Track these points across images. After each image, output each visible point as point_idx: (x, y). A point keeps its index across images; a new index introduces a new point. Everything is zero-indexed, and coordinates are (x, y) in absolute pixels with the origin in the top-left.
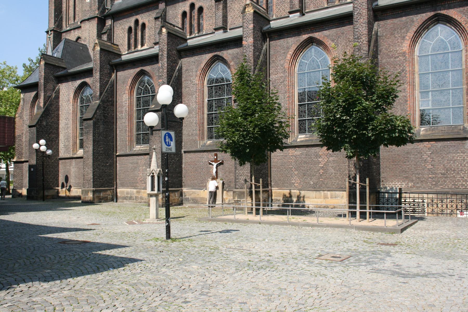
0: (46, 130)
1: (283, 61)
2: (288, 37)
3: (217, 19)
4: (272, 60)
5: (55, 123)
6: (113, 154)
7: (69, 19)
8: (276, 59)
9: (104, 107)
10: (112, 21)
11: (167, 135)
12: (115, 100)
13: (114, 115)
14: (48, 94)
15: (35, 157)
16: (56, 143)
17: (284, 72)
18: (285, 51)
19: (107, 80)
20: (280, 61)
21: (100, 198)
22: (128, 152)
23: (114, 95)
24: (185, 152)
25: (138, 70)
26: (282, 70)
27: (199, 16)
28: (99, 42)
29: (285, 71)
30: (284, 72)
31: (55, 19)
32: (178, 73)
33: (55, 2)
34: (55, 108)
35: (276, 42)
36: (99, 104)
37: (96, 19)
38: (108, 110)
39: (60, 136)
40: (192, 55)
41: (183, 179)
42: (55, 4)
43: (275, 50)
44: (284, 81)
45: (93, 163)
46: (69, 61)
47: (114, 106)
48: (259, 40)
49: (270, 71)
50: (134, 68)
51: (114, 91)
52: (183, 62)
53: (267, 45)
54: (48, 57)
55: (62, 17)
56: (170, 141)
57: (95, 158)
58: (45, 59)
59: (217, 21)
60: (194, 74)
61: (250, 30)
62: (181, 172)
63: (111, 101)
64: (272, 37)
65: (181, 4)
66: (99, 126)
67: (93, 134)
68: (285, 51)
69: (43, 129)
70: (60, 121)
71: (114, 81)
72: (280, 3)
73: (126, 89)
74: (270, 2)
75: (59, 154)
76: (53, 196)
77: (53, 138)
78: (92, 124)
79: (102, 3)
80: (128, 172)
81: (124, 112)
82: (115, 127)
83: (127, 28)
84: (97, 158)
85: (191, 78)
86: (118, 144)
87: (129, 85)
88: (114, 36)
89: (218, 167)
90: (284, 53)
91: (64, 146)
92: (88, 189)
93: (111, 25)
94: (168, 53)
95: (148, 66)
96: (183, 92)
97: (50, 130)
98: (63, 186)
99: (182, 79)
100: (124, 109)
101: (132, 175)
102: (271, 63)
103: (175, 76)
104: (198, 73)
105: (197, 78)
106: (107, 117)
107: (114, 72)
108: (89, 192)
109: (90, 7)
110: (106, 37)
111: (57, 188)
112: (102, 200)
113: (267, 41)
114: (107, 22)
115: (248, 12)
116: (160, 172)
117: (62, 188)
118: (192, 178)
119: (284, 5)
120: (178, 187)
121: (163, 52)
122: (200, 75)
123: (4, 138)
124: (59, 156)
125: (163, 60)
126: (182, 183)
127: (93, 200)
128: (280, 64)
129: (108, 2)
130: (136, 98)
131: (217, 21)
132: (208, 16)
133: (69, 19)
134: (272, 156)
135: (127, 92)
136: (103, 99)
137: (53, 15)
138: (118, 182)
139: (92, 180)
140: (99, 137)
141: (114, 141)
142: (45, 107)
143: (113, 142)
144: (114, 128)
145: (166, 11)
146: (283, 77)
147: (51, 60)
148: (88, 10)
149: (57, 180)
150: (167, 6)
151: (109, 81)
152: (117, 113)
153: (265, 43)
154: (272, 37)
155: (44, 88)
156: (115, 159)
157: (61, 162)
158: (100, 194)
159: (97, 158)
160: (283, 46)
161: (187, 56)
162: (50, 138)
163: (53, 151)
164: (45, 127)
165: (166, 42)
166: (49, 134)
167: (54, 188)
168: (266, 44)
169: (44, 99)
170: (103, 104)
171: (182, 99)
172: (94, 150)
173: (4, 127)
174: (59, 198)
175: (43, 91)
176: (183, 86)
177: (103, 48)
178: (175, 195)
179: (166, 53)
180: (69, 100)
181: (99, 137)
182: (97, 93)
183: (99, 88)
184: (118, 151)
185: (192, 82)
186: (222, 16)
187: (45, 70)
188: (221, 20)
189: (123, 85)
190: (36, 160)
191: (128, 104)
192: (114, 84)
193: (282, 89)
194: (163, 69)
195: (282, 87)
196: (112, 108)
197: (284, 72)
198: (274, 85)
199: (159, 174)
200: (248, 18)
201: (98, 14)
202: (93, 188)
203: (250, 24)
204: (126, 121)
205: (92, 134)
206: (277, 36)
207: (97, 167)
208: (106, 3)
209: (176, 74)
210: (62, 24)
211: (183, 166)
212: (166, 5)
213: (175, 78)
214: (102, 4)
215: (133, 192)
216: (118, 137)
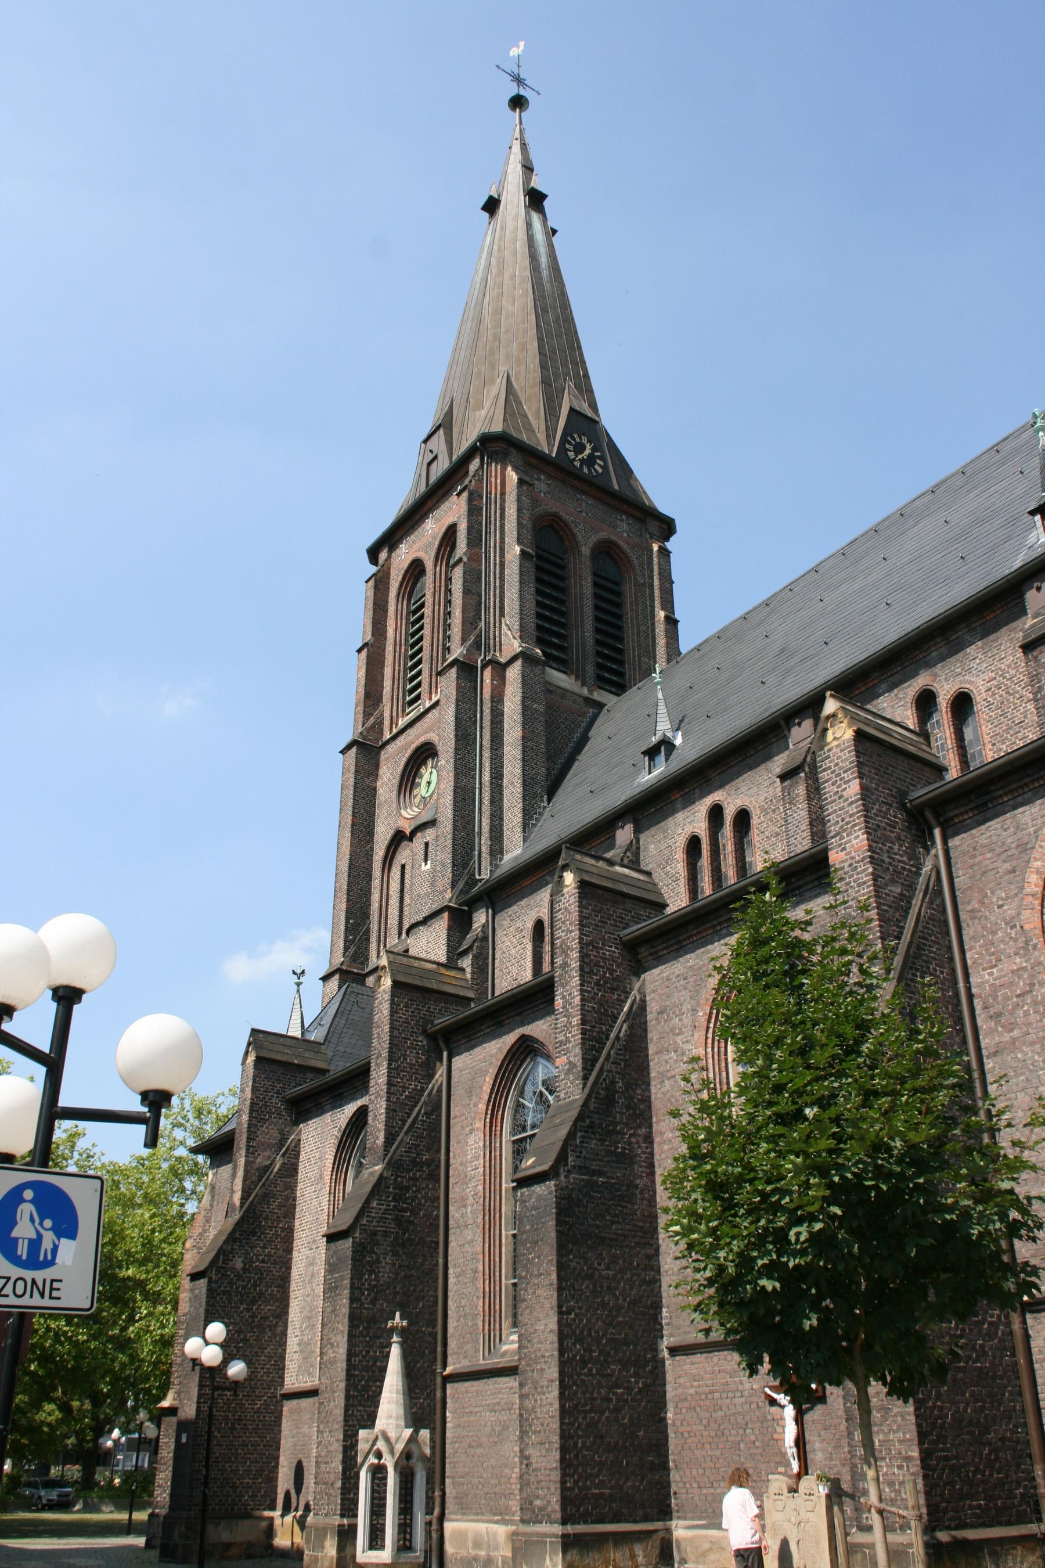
0: (244, 1288)
1: (1014, 905)
2: (1015, 807)
3: (791, 833)
4: (969, 908)
5: (275, 1263)
6: (434, 1372)
7: (386, 933)
8: (981, 903)
9: (399, 1187)
10: (490, 911)
11: (28, 1194)
12: (443, 1158)
13: (438, 1216)
14: (259, 1160)
15: (196, 1389)
16: (275, 1335)
17: (1025, 948)
18: (1015, 863)
19: (414, 1089)
20: (1000, 907)
22: (482, 1362)
23: (440, 1142)
24: (674, 1351)
25: (510, 1039)
26: (1015, 940)
27: (742, 843)
28: (390, 963)
29: (1027, 943)
30: (1026, 948)
31: (346, 937)
32: (630, 1027)
33: (348, 890)
34: (280, 1207)
35: (973, 837)
36: (381, 1175)
37: (446, 915)
38: (413, 1199)
39: (290, 1309)
40: (677, 950)
41: (674, 1476)
42: (348, 894)
43: (971, 867)
44: (1032, 985)
45: (346, 1410)
46: (349, 1050)
47: (438, 1181)
48: (899, 838)
49: (968, 955)
50: (500, 1036)
51: (440, 1125)
52: (647, 983)
53: (936, 856)
54: (270, 1038)
55: (368, 931)
56: (48, 1239)
58: (256, 1048)
59: (792, 841)
60: (685, 1021)
61: (852, 803)
62: (659, 1446)
63: (428, 1163)
64: (952, 818)
65: (680, 816)
66: (378, 1261)
67: (352, 1293)
68: (1015, 863)
70: (295, 1254)
71: (439, 1091)
72: (1007, 731)
73: (476, 1113)
74: (971, 741)
75: (282, 1378)
76: (250, 1545)
77: (266, 1318)
78: (349, 1253)
79: (465, 865)
80: (480, 1445)
81: (471, 1200)
82: (441, 1261)
83: (530, 925)
85: (679, 1039)
86: (451, 1330)
87: (487, 1098)
88: (494, 959)
89: (807, 1417)
90: (1014, 871)
91: (299, 1344)
92: (327, 1520)
93: (484, 926)
94: (583, 957)
95: (541, 1018)
96: (653, 1097)
97: (255, 1285)
98: (287, 1509)
99: (647, 1049)
100: (469, 1191)
101: (493, 1462)
102: (963, 925)
103: (617, 1038)
104: (702, 1015)
105: (696, 1035)
106: (412, 1222)
107: (441, 1060)
108: (325, 1536)
109: (432, 884)
110: (470, 962)
111: (267, 1513)
113: (934, 843)
114: (475, 919)
115: (835, 743)
116: (414, 1447)
117: (283, 1516)
118: (708, 1472)
119: (1020, 735)
120: (646, 1519)
121: (567, 955)
122: (709, 1021)
124: (282, 1384)
125: (567, 983)
126: (668, 1496)
128: (1004, 919)
129: (483, 863)
130: (510, 1145)
131: (792, 841)
132: (767, 834)
133: (386, 933)
134: (1034, 1350)
135: (479, 1125)
136: (396, 1156)
137: (343, 928)
138: (448, 1491)
139: (339, 1484)
140: (373, 1302)
141: (436, 1320)
142: (244, 1209)
143: (433, 1323)
144: (437, 1265)
145: (638, 848)
146: (1024, 969)
148: (427, 895)
149: (272, 1480)
150: (641, 832)
151: (423, 1090)
152: (451, 1208)
153: (927, 850)
154: (952, 818)
155: (249, 1139)
156: (439, 1394)
157: (288, 1406)
160: (1003, 843)
161: (659, 960)
162: (253, 1316)
163: (249, 1364)
164: (239, 1276)
165: (575, 915)
166: (254, 1302)
167: (257, 1513)
168: (933, 852)
169: (244, 1181)
170: (397, 1176)
171: (650, 1126)
172: (350, 1355)
174: (271, 1555)
175: (243, 1152)
176: (653, 1074)
177: (401, 978)
178: (633, 1557)
179: (575, 954)
180: (321, 1177)
181: (373, 1302)
182: (377, 1138)
183: (383, 1116)
184: (450, 1360)
185: (683, 1054)
186: (807, 822)
187: (254, 1081)
188: (805, 834)
189: (467, 1101)
190: (198, 1402)
191: (481, 1170)
192: (441, 1101)
193: (1030, 1024)
194: (568, 1016)
195: (1026, 1014)
196: (434, 1188)
197: (1025, 948)
198: (992, 1011)
199: (407, 1455)
200: (837, 765)
201: (450, 900)
202: (342, 1516)
203: (849, 781)
204: (475, 1233)
205: (347, 1292)
206: (972, 810)
208: (477, 866)
209: (620, 1028)
210: (367, 949)
211: (669, 1415)
212: (638, 830)
213: (617, 1046)
214: (464, 868)
215: (495, 1534)
216: (450, 1303)
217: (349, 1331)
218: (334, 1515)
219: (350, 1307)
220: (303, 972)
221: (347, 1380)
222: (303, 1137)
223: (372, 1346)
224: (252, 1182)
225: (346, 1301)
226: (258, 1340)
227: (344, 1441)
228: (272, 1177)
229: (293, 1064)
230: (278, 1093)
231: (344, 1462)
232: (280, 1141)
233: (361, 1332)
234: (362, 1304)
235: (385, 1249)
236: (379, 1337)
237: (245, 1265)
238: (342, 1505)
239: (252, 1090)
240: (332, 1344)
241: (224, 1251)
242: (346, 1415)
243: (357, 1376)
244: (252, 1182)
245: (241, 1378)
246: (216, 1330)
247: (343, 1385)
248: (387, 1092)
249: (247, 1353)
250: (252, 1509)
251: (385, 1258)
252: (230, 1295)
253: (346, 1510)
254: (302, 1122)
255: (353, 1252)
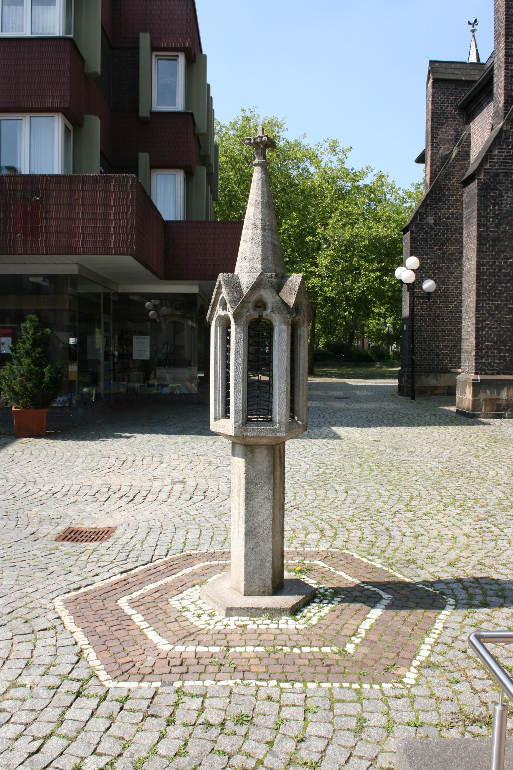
14: (441, 151)
21: (499, 406)
54: (444, 65)
57: (484, 287)
66: (501, 195)
69: (426, 233)
77: (453, 254)
84: (493, 288)
112: (505, 410)
123: (107, 234)
127: (474, 409)
139: (474, 353)
147: (449, 71)
158: (498, 394)
159: (493, 288)
162: (444, 253)
164: (432, 229)
166: (443, 244)
167: (453, 370)
173: (107, 205)
181: (498, 226)
202: (476, 374)
207: (492, 315)
217: (477, 248)
218: (472, 373)
219: (478, 231)
220: (476, 21)
221: (477, 283)
222: (472, 131)
223: (497, 259)
224: (437, 167)
225: (475, 227)
226: (448, 267)
227: (476, 324)
228: (451, 161)
229: (462, 81)
230: (452, 103)
231: (476, 338)
232: (456, 136)
233: (487, 248)
234: (488, 228)
235: (507, 186)
236: (503, 252)
237: (435, 221)
238: (476, 366)
239: (432, 103)
240: (468, 259)
241: (420, 213)
242: (477, 307)
243: (486, 279)
244: (437, 167)
245: (432, 290)
246: (413, 262)
247: (474, 286)
248: (505, 63)
249: (441, 276)
250: (450, 368)
251: (507, 193)
252: (426, 241)
253: (479, 370)
254: (471, 121)
255: (479, 190)
